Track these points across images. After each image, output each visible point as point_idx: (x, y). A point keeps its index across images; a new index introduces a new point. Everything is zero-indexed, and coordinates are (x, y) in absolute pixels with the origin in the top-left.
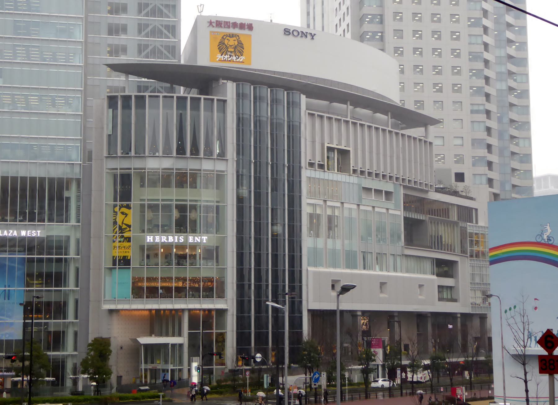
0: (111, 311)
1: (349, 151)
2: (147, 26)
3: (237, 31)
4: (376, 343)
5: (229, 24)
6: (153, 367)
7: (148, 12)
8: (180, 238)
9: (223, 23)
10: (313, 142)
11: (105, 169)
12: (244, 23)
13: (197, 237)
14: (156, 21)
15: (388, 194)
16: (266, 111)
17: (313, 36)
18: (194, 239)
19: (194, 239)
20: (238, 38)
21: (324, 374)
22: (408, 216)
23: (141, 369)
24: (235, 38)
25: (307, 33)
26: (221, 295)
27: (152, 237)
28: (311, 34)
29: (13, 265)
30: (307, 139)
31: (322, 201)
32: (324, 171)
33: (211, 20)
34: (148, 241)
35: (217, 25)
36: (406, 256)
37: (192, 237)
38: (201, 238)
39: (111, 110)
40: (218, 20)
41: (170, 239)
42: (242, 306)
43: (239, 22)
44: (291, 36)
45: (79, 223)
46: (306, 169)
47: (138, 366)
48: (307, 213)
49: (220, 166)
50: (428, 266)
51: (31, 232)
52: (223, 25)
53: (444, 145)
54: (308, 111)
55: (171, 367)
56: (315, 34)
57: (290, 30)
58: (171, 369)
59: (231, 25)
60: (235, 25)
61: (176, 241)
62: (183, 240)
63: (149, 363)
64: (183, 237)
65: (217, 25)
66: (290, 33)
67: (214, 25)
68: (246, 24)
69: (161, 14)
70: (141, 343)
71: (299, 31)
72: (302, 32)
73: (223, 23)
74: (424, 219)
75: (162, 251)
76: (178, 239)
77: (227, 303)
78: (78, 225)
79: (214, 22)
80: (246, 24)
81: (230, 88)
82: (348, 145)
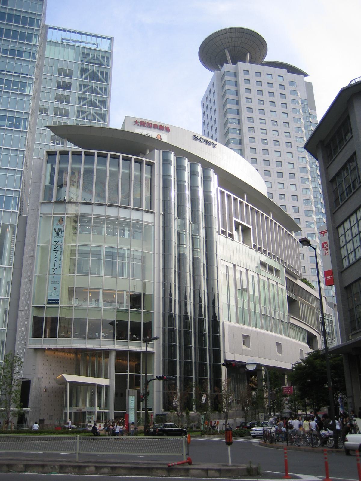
0: (36, 350)
1: (249, 228)
2: (87, 70)
4: (288, 392)
5: (150, 125)
6: (78, 410)
7: (88, 76)
9: (146, 123)
11: (40, 214)
14: (93, 96)
15: (277, 271)
21: (262, 416)
23: (66, 413)
25: (210, 142)
26: (148, 338)
31: (232, 265)
33: (136, 121)
39: (49, 165)
42: (169, 350)
43: (159, 125)
44: (198, 142)
45: (11, 266)
47: (62, 410)
49: (148, 218)
54: (219, 188)
55: (97, 409)
56: (216, 144)
57: (198, 137)
58: (97, 412)
63: (74, 406)
66: (198, 139)
68: (165, 126)
69: (95, 105)
70: (67, 380)
71: (205, 139)
73: (146, 123)
75: (90, 295)
77: (153, 347)
78: (10, 268)
79: (139, 122)
80: (165, 126)
81: (157, 156)
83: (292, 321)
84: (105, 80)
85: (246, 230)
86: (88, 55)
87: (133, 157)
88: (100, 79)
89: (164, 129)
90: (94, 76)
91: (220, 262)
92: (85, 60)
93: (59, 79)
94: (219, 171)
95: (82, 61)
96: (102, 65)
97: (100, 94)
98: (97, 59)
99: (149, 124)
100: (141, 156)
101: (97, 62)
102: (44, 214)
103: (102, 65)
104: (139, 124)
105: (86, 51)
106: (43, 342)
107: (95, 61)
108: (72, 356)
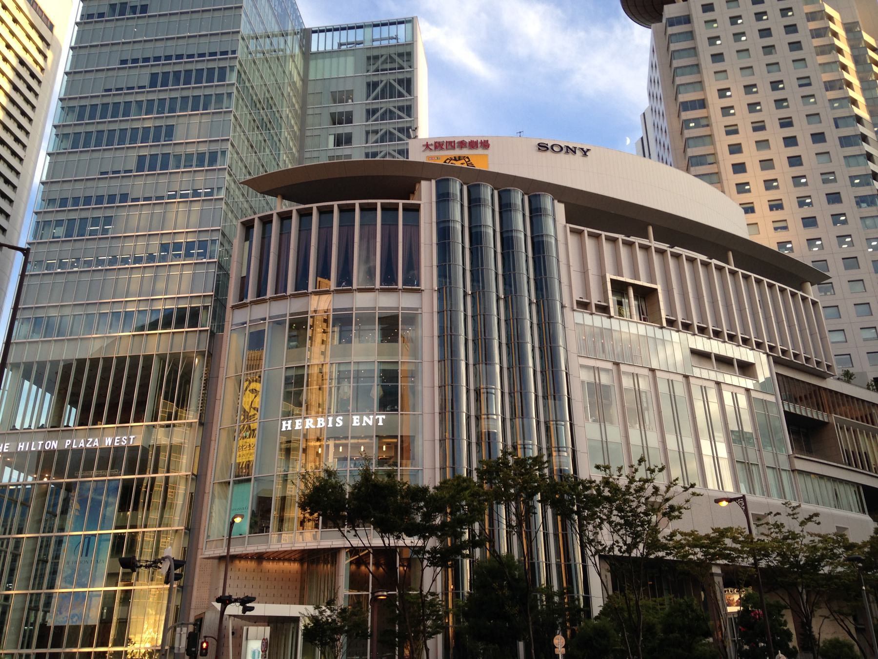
1: (656, 290)
3: (465, 152)
8: (338, 420)
9: (445, 144)
10: (584, 272)
12: (475, 140)
13: (368, 415)
16: (671, 442)
17: (585, 153)
18: (361, 421)
19: (361, 421)
20: (467, 160)
22: (792, 410)
24: (463, 161)
25: (575, 148)
27: (290, 422)
28: (582, 149)
29: (99, 497)
30: (571, 264)
32: (610, 317)
34: (284, 429)
35: (436, 148)
36: (801, 472)
37: (358, 417)
38: (373, 418)
40: (438, 140)
41: (319, 423)
43: (467, 140)
44: (549, 154)
46: (574, 310)
48: (583, 382)
50: (849, 496)
51: (121, 439)
52: (444, 147)
53: (846, 342)
54: (569, 225)
56: (588, 150)
59: (456, 145)
60: (462, 144)
61: (330, 425)
62: (341, 423)
64: (341, 418)
65: (436, 148)
66: (548, 149)
67: (432, 147)
68: (479, 141)
71: (563, 146)
72: (568, 147)
74: (826, 420)
76: (334, 422)
79: (432, 145)
80: (479, 141)
82: (652, 278)
83: (800, 465)
84: (407, 92)
85: (646, 295)
86: (376, 58)
87: (401, 202)
88: (399, 92)
89: (479, 145)
90: (389, 91)
91: (576, 362)
92: (373, 68)
93: (333, 110)
94: (561, 193)
95: (368, 71)
96: (401, 68)
97: (400, 117)
98: (393, 61)
99: (450, 143)
100: (411, 198)
101: (393, 66)
102: (237, 325)
103: (401, 68)
104: (431, 147)
105: (375, 53)
106: (246, 543)
107: (388, 66)
108: (295, 566)
